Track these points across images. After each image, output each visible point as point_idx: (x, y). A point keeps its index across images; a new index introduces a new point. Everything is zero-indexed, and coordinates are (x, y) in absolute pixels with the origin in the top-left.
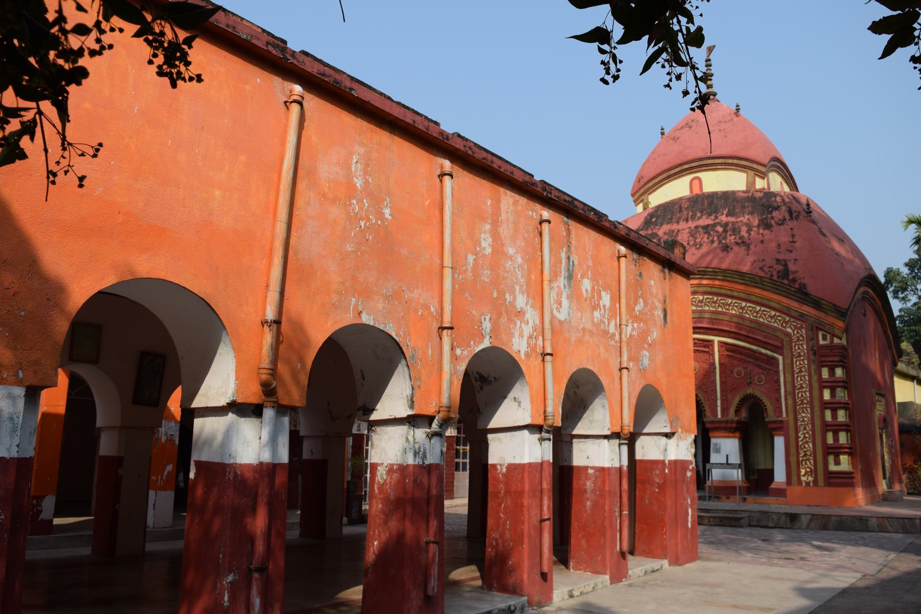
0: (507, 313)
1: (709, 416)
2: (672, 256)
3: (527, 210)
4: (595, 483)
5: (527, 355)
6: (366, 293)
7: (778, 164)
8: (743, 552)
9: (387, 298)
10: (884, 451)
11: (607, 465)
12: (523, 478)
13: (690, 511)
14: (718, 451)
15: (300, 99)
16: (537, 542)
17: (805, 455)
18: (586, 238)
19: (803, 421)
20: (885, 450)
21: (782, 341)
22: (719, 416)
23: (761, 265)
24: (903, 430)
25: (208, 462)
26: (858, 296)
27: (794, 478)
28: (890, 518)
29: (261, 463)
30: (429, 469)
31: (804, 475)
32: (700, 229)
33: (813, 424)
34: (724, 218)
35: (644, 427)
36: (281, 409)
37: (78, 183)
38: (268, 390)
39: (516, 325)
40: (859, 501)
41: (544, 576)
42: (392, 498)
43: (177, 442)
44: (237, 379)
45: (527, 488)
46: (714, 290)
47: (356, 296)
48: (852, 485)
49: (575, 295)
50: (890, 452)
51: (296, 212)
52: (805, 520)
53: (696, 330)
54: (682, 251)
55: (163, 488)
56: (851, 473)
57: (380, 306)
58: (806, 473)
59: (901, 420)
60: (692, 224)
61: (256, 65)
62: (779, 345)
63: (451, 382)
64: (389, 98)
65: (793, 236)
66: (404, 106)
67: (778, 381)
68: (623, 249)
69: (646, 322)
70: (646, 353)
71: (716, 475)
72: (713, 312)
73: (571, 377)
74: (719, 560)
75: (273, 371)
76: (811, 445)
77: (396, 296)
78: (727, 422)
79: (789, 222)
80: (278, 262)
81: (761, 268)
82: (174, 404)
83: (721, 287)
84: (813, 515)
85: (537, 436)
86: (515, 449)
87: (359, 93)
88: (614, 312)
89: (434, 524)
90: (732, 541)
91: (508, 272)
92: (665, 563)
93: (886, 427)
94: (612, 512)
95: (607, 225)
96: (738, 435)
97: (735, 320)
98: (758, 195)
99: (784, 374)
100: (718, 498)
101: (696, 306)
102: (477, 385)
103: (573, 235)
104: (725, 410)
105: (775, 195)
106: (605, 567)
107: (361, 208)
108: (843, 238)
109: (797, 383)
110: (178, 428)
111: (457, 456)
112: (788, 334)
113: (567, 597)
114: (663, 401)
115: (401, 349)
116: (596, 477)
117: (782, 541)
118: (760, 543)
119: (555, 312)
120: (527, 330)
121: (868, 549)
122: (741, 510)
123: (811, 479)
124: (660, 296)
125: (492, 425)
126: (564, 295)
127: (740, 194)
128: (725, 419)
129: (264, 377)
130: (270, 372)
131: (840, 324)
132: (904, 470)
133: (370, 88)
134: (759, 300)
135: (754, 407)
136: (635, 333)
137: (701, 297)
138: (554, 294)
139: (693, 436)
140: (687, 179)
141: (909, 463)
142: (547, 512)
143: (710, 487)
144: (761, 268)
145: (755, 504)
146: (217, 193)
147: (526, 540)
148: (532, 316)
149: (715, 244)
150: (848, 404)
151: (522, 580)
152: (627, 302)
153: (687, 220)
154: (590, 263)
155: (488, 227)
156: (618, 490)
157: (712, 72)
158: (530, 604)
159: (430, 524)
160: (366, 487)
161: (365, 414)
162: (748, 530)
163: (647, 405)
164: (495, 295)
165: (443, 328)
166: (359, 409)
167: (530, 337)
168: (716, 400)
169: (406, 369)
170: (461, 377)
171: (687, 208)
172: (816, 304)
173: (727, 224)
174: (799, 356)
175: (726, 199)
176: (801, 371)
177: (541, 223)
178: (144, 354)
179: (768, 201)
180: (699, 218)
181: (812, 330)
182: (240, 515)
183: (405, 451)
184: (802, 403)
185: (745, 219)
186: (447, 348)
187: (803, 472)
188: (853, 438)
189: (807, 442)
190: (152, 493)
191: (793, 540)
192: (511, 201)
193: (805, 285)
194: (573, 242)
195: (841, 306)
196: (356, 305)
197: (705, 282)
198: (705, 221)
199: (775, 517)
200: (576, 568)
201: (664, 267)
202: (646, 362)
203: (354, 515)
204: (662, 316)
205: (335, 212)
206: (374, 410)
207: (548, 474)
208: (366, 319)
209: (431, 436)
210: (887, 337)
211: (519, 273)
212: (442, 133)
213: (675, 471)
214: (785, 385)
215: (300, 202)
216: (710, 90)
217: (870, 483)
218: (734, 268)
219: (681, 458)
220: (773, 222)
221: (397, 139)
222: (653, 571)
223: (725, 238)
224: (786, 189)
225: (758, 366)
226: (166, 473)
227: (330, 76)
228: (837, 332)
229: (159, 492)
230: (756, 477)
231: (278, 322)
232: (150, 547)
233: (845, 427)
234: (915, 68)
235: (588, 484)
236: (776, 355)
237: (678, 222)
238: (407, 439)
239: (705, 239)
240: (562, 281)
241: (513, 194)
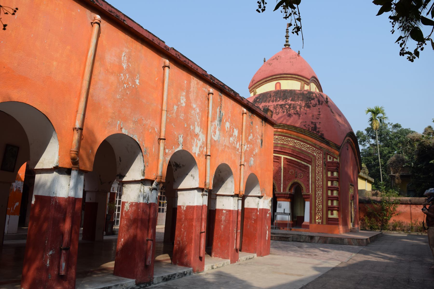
0: (191, 135)
1: (277, 191)
2: (266, 115)
3: (203, 87)
4: (226, 217)
5: (199, 155)
6: (125, 119)
7: (315, 80)
8: (290, 252)
9: (135, 122)
10: (352, 210)
11: (232, 209)
12: (193, 212)
13: (267, 232)
14: (280, 207)
15: (99, 22)
16: (199, 242)
17: (319, 210)
18: (229, 103)
19: (319, 195)
20: (353, 210)
21: (312, 159)
22: (282, 191)
24: (361, 202)
25: (42, 196)
26: (346, 141)
27: (313, 220)
28: (353, 239)
29: (69, 197)
30: (150, 205)
31: (317, 219)
33: (323, 196)
34: (289, 102)
35: (249, 193)
36: (81, 172)
37: (3, 27)
38: (75, 162)
39: (194, 140)
40: (340, 231)
41: (201, 258)
42: (132, 218)
43: (22, 191)
44: (59, 155)
45: (195, 217)
46: (283, 134)
47: (120, 120)
48: (338, 224)
49: (222, 129)
50: (354, 211)
51: (93, 77)
52: (317, 239)
53: (275, 152)
54: (271, 114)
55: (13, 214)
56: (338, 219)
57: (131, 126)
58: (318, 218)
59: (360, 197)
60: (275, 103)
61: (78, 3)
62: (310, 160)
63: (163, 165)
64: (142, 27)
65: (319, 112)
66: (148, 32)
67: (309, 177)
68: (245, 110)
69: (253, 145)
70: (252, 159)
71: (279, 218)
72: (282, 144)
73: (218, 168)
74: (279, 255)
75: (78, 153)
76: (321, 206)
77: (139, 122)
78: (285, 194)
79: (318, 106)
80: (83, 100)
81: (304, 126)
82: (22, 172)
83: (286, 133)
85: (201, 193)
86: (190, 199)
87: (127, 23)
88: (239, 139)
89: (151, 231)
90: (285, 247)
91: (192, 115)
92: (255, 255)
93: (353, 200)
94: (233, 230)
95: (239, 98)
96: (289, 200)
97: (291, 148)
98: (305, 92)
99: (312, 173)
100: (279, 228)
101: (275, 141)
102: (174, 168)
103: (223, 101)
105: (313, 93)
106: (228, 256)
107: (125, 78)
108: (341, 115)
109: (317, 179)
110: (23, 185)
111: (160, 205)
112: (314, 156)
113: (210, 268)
114: (258, 181)
115: (140, 147)
116: (227, 214)
117: (307, 248)
118: (297, 248)
119: (213, 136)
120: (199, 143)
121: (344, 252)
122: (290, 234)
123: (320, 221)
124: (260, 133)
125: (180, 187)
126: (217, 129)
127: (298, 91)
128: (284, 193)
129: (73, 155)
130: (76, 153)
131: (337, 152)
132: (360, 219)
133: (133, 21)
134: (303, 140)
135: (297, 187)
136: (248, 149)
137: (277, 137)
138: (213, 128)
139: (271, 198)
140: (274, 83)
141: (362, 216)
142: (204, 229)
143: (276, 223)
144: (304, 126)
145: (295, 231)
146: (55, 63)
147: (193, 241)
148: (202, 137)
149: (285, 113)
150: (338, 188)
151: (190, 260)
152: (245, 135)
153: (273, 101)
154: (230, 115)
155: (184, 93)
156: (236, 221)
158: (194, 271)
159: (149, 231)
160: (115, 218)
161: (120, 178)
162: (292, 243)
163: (252, 182)
164: (186, 126)
165: (160, 139)
166: (117, 176)
167: (201, 147)
168: (281, 184)
169: (142, 157)
170: (168, 163)
171: (273, 96)
173: (291, 105)
174: (319, 166)
175: (291, 93)
176: (319, 173)
177: (209, 94)
178: (8, 146)
179: (309, 95)
180: (278, 101)
181: (325, 154)
182: (57, 223)
183: (139, 196)
184: (319, 187)
185: (299, 103)
186: (162, 148)
187: (317, 217)
188: (339, 204)
189: (319, 205)
190: (8, 216)
191: (311, 247)
192: (196, 82)
193: (323, 134)
194: (223, 105)
195: (338, 144)
196: (120, 125)
197: (279, 130)
198: (281, 102)
199: (304, 237)
200: (215, 256)
201: (263, 120)
202: (252, 163)
203: (109, 231)
204: (260, 143)
205: (112, 78)
206: (125, 176)
207: (205, 211)
208: (124, 131)
209: (152, 190)
210: (356, 160)
211: (197, 117)
212: (166, 47)
213: (262, 214)
214: (312, 178)
215: (95, 72)
216: (287, 43)
217: (345, 224)
218: (293, 124)
219: (265, 208)
220: (311, 105)
221: (144, 47)
222: (250, 259)
223: (289, 111)
224: (318, 91)
225: (300, 169)
226: (15, 206)
227: (114, 13)
228: (336, 156)
229: (11, 216)
230: (296, 220)
231: (81, 129)
232: (5, 242)
233: (337, 199)
234: (390, 22)
235: (223, 217)
236: (308, 165)
237: (269, 102)
238: (140, 190)
239: (281, 111)
240: (217, 122)
241: (197, 79)
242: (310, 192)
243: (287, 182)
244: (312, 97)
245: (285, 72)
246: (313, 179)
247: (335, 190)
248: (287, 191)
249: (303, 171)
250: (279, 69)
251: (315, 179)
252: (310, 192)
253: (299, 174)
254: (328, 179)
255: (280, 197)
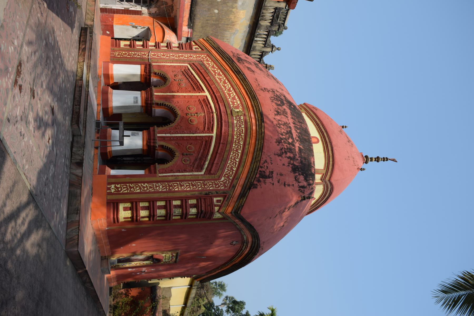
17: (131, 188)
19: (156, 187)
21: (214, 174)
22: (158, 135)
23: (269, 161)
27: (113, 180)
31: (115, 187)
32: (289, 129)
33: (154, 192)
34: (297, 145)
52: (78, 172)
58: (118, 188)
60: (292, 125)
62: (212, 172)
76: (139, 191)
78: (154, 139)
81: (266, 161)
84: (82, 178)
99: (191, 175)
101: (237, 123)
104: (163, 138)
109: (184, 183)
112: (220, 178)
123: (113, 191)
134: (243, 160)
145: (91, 155)
153: (294, 123)
157: (380, 161)
168: (170, 134)
172: (243, 195)
174: (205, 185)
184: (170, 186)
189: (140, 188)
193: (256, 188)
195: (243, 210)
199: (80, 152)
214: (183, 175)
220: (297, 174)
225: (196, 160)
237: (292, 118)
239: (283, 131)
242: (160, 175)
243: (173, 142)
244: (308, 179)
245: (335, 148)
246: (182, 178)
247: (167, 211)
248: (159, 143)
249: (194, 164)
250: (336, 141)
251: (182, 181)
252: (160, 175)
253: (187, 158)
254: (184, 200)
255: (149, 134)
